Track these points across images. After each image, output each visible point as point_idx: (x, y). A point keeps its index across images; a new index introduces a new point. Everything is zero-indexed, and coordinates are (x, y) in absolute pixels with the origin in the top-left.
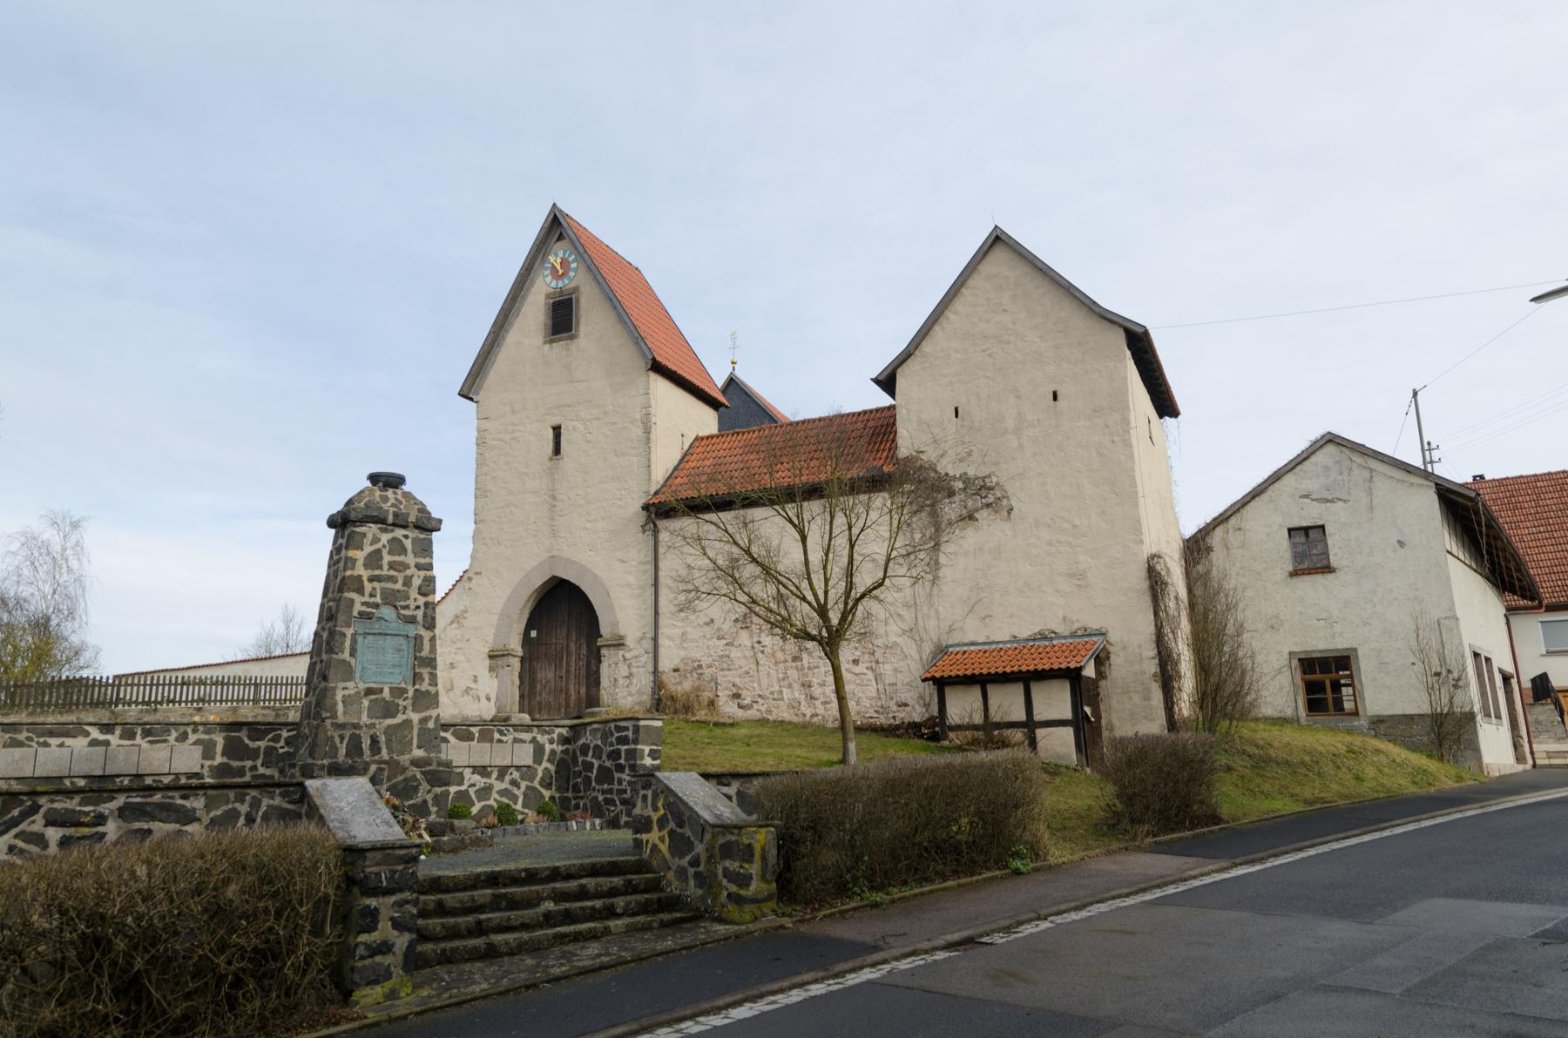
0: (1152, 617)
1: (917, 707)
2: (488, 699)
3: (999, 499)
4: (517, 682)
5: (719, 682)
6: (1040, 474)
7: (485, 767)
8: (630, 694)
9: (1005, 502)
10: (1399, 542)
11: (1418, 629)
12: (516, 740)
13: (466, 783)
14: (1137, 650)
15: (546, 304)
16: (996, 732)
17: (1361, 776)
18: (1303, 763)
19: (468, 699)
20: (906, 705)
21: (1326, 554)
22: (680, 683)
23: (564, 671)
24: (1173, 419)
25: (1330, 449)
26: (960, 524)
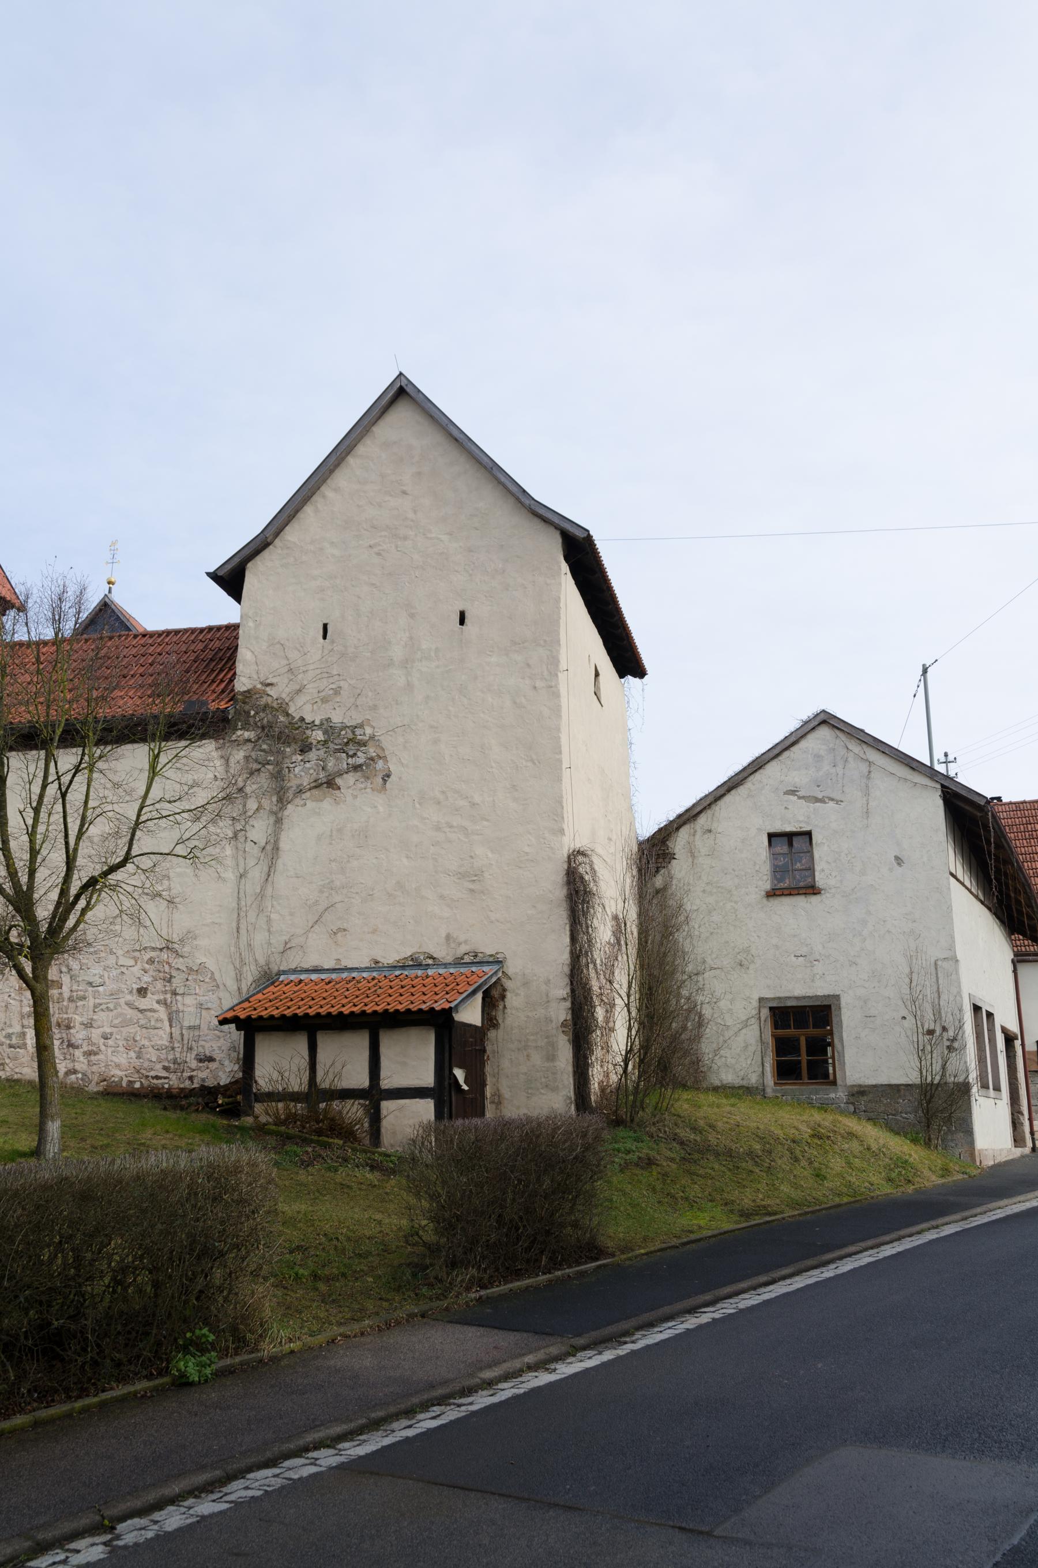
0: (568, 940)
1: (227, 1063)
3: (372, 759)
6: (432, 727)
9: (380, 764)
10: (897, 858)
11: (912, 973)
14: (543, 987)
16: (322, 1105)
17: (823, 1172)
18: (751, 1154)
20: (211, 1059)
21: (811, 869)
24: (637, 679)
25: (824, 732)
26: (315, 792)
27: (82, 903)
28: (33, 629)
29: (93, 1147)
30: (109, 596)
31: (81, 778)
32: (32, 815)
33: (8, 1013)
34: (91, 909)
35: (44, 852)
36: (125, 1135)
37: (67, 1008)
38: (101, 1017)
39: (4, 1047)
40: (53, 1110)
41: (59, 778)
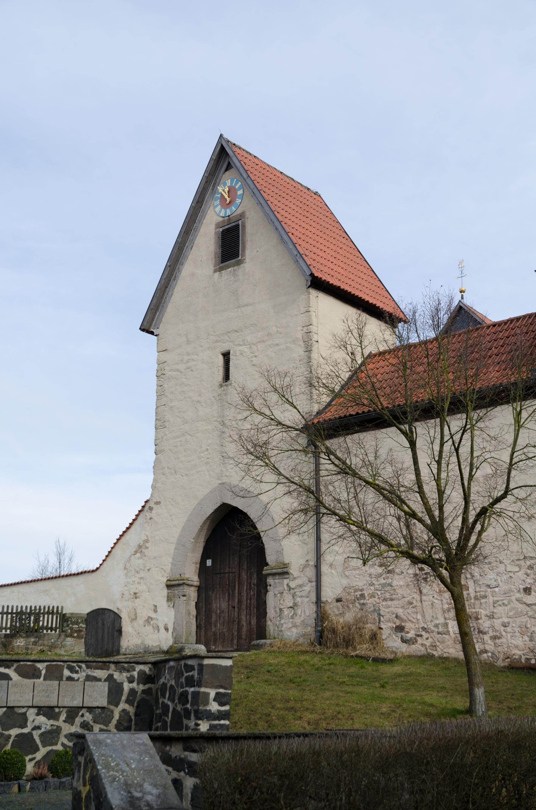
2: (167, 629)
4: (194, 612)
5: (382, 613)
7: (52, 708)
8: (295, 626)
12: (89, 678)
13: (30, 726)
15: (216, 233)
19: (149, 629)
22: (342, 614)
23: (236, 601)
27: (478, 527)
28: (422, 334)
29: (509, 708)
30: (462, 301)
31: (467, 436)
32: (436, 466)
33: (434, 609)
34: (485, 531)
35: (448, 492)
36: (530, 700)
37: (474, 604)
38: (499, 610)
39: (434, 633)
40: (477, 679)
41: (452, 437)
